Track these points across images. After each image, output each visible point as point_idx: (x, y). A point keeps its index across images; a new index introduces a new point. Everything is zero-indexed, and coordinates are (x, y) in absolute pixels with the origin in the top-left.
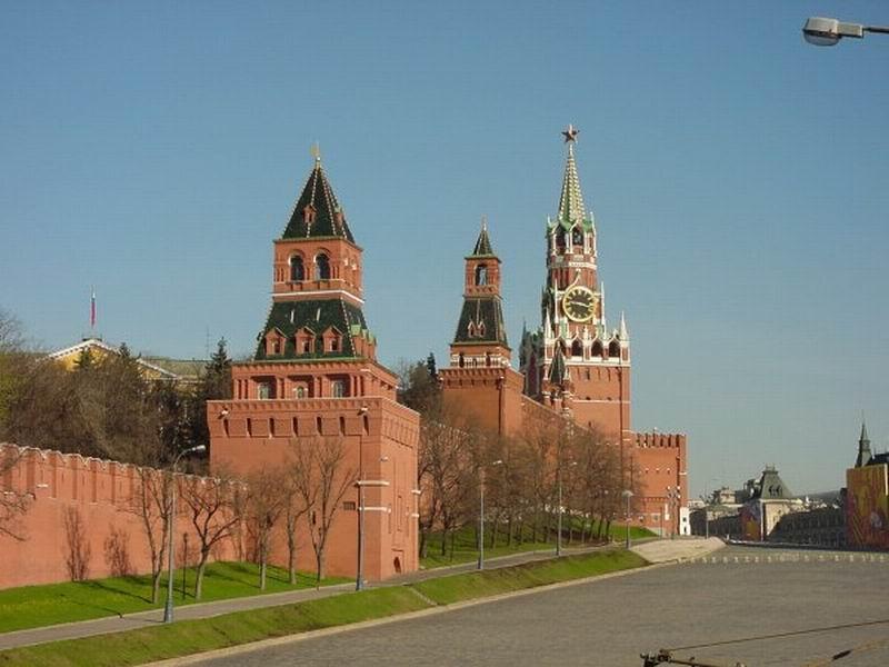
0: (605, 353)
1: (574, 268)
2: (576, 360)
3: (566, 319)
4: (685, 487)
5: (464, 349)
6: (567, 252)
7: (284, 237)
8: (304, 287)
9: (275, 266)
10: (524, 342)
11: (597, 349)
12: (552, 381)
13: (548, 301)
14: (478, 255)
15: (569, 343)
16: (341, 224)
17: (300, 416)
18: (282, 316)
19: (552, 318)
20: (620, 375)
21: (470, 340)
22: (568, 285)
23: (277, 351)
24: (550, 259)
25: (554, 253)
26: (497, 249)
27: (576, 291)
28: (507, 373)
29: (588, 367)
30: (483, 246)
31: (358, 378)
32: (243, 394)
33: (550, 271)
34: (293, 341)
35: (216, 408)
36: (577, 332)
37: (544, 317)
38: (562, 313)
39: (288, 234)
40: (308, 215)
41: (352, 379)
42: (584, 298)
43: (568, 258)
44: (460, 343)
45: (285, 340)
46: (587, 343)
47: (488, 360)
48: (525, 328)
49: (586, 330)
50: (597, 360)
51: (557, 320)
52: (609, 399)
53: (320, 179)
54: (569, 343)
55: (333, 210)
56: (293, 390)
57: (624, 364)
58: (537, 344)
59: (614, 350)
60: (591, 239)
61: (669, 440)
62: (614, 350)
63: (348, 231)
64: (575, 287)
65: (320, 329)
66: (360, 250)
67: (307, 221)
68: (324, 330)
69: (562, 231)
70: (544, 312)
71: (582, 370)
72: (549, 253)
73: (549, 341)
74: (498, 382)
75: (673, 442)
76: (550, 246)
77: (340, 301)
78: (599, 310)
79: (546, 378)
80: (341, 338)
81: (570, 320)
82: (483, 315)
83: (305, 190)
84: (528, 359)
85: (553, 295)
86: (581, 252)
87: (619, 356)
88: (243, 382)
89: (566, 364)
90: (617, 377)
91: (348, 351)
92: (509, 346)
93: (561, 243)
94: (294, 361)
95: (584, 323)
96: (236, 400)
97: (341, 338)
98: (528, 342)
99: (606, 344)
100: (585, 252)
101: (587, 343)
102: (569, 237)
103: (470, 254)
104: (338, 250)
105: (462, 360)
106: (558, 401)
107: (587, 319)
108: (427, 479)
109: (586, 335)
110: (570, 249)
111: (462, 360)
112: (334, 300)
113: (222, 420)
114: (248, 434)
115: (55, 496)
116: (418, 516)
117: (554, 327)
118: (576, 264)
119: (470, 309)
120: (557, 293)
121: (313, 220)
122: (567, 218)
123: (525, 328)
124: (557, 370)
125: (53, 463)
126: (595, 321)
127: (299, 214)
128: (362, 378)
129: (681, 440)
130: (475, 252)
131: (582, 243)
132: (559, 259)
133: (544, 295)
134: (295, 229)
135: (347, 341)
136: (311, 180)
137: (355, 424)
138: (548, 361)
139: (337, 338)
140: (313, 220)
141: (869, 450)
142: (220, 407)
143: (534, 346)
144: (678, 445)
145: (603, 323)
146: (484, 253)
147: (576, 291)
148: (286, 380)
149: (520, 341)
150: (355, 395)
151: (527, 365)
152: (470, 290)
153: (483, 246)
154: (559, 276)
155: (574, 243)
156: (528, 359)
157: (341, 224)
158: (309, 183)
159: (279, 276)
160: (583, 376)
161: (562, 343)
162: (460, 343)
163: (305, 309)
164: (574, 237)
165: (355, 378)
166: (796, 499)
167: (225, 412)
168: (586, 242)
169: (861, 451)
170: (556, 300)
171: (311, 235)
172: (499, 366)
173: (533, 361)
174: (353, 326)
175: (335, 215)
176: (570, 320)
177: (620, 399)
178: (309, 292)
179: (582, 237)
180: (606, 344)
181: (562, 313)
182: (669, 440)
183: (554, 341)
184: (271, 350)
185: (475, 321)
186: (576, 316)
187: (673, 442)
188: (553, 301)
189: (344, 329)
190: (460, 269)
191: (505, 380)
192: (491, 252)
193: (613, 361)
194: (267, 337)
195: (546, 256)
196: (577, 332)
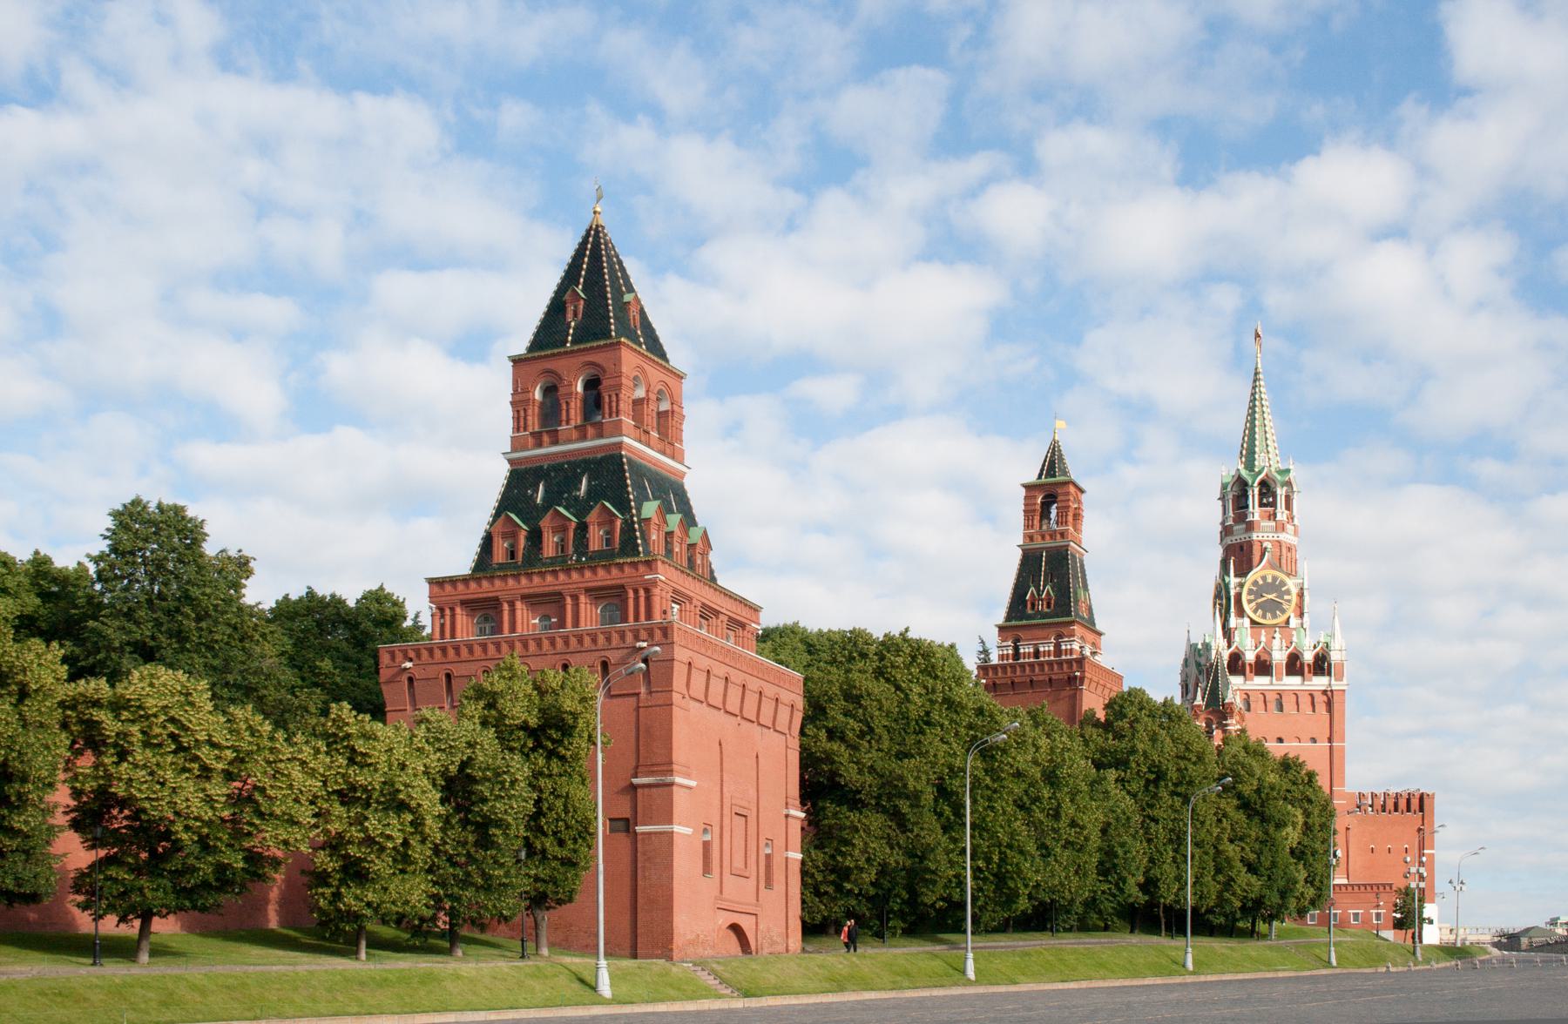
3: (1247, 621)
4: (1431, 871)
8: (561, 437)
11: (1294, 665)
12: (1207, 706)
13: (1221, 593)
20: (1329, 704)
21: (1030, 617)
22: (1250, 569)
23: (513, 555)
26: (1075, 469)
27: (1264, 578)
29: (1280, 694)
30: (1053, 463)
32: (448, 634)
34: (536, 537)
35: (393, 658)
36: (1263, 639)
38: (1241, 613)
39: (538, 343)
41: (631, 594)
42: (1276, 586)
43: (1250, 527)
44: (1013, 623)
46: (1279, 656)
47: (1058, 646)
49: (1277, 635)
50: (1294, 682)
52: (1314, 740)
53: (596, 245)
56: (528, 622)
57: (1336, 686)
58: (1203, 661)
59: (1321, 665)
61: (1408, 801)
62: (1321, 665)
65: (581, 509)
66: (1100, 634)
71: (1272, 698)
74: (1072, 680)
75: (1415, 803)
80: (619, 523)
81: (1253, 622)
90: (1324, 707)
91: (629, 545)
92: (1099, 627)
93: (1241, 502)
95: (1275, 626)
97: (619, 523)
99: (1308, 657)
101: (1279, 656)
103: (1032, 477)
104: (618, 363)
105: (1016, 649)
106: (1217, 734)
107: (1281, 619)
109: (1276, 643)
110: (1255, 512)
111: (1016, 649)
112: (612, 456)
113: (404, 678)
116: (800, 856)
119: (1029, 563)
120: (1233, 580)
122: (1250, 465)
126: (1294, 622)
127: (557, 308)
128: (647, 591)
130: (1040, 477)
131: (1274, 504)
134: (549, 333)
135: (628, 528)
142: (399, 656)
143: (1198, 665)
144: (1421, 809)
147: (1264, 578)
148: (519, 605)
150: (637, 619)
153: (1053, 463)
155: (1261, 505)
159: (519, 422)
160: (1272, 706)
162: (1013, 623)
163: (560, 476)
164: (1261, 494)
165: (636, 592)
167: (408, 665)
168: (1281, 502)
170: (1232, 593)
171: (573, 342)
175: (623, 307)
176: (1253, 622)
177: (1330, 740)
180: (1308, 657)
181: (1241, 613)
182: (1408, 801)
184: (499, 555)
186: (1264, 617)
187: (1415, 803)
188: (1228, 592)
189: (623, 506)
191: (1082, 679)
193: (1320, 682)
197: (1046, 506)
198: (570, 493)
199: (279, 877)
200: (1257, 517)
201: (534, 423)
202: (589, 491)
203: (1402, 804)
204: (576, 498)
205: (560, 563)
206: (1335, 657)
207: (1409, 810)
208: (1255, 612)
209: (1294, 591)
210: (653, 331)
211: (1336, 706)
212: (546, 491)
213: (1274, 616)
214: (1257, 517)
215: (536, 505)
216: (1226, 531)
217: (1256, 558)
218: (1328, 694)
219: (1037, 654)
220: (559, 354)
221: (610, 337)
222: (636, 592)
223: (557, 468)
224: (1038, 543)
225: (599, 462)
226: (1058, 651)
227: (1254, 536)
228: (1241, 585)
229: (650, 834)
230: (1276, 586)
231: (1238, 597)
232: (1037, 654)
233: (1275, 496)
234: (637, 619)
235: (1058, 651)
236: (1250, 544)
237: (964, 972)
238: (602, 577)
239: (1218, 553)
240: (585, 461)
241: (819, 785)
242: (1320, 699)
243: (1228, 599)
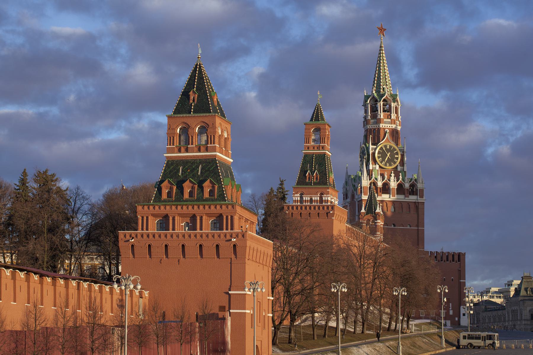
0: (406, 192)
1: (384, 129)
2: (385, 197)
3: (377, 166)
5: (304, 190)
6: (379, 117)
7: (175, 113)
10: (346, 183)
15: (380, 184)
16: (216, 104)
17: (204, 244)
19: (367, 165)
28: (335, 208)
31: (229, 217)
33: (367, 130)
38: (375, 162)
39: (177, 111)
43: (379, 121)
45: (175, 187)
47: (321, 198)
48: (347, 173)
51: (371, 167)
54: (380, 184)
57: (420, 200)
60: (396, 107)
61: (447, 257)
63: (221, 109)
64: (386, 142)
67: (191, 101)
68: (204, 181)
70: (362, 161)
72: (365, 117)
73: (365, 182)
75: (456, 258)
76: (366, 112)
77: (216, 160)
79: (363, 211)
80: (216, 187)
81: (380, 167)
82: (323, 200)
84: (349, 195)
85: (368, 149)
86: (389, 117)
87: (417, 194)
88: (145, 218)
89: (378, 199)
91: (222, 197)
93: (374, 110)
94: (182, 203)
96: (140, 231)
98: (350, 183)
100: (392, 118)
108: (280, 288)
109: (392, 178)
110: (382, 115)
111: (301, 197)
114: (131, 256)
115: (15, 301)
116: (271, 315)
118: (386, 126)
123: (347, 173)
124: (371, 205)
125: (28, 280)
129: (461, 257)
131: (389, 110)
133: (362, 148)
136: (195, 71)
137: (226, 251)
138: (365, 197)
139: (213, 187)
147: (385, 146)
149: (344, 182)
150: (142, 229)
151: (349, 200)
155: (384, 111)
156: (349, 195)
157: (216, 104)
161: (375, 184)
168: (393, 110)
170: (371, 153)
172: (329, 204)
173: (353, 196)
174: (226, 179)
179: (390, 106)
181: (375, 162)
182: (447, 257)
183: (369, 182)
187: (456, 258)
188: (368, 152)
189: (219, 182)
191: (333, 214)
195: (363, 120)
203: (450, 258)
206: (419, 186)
207: (453, 261)
214: (382, 117)
216: (366, 122)
217: (381, 138)
219: (311, 201)
220: (189, 117)
226: (321, 201)
227: (382, 125)
228: (375, 149)
231: (374, 154)
232: (311, 201)
234: (142, 229)
235: (321, 201)
236: (379, 129)
239: (362, 132)
243: (369, 155)
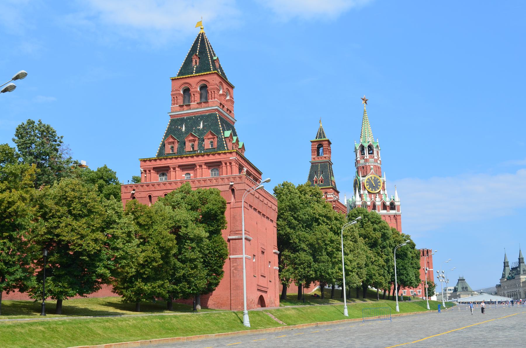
0: (388, 208)
3: (366, 192)
6: (365, 158)
7: (179, 75)
9: (172, 95)
11: (384, 207)
14: (318, 139)
18: (177, 130)
24: (357, 162)
25: (359, 159)
30: (321, 134)
36: (373, 198)
37: (355, 190)
40: (194, 61)
46: (378, 203)
49: (377, 196)
51: (362, 192)
53: (203, 39)
55: (212, 57)
59: (392, 206)
61: (423, 252)
62: (392, 206)
69: (362, 148)
70: (355, 190)
75: (425, 253)
78: (383, 187)
81: (368, 192)
83: (193, 47)
92: (338, 189)
99: (388, 204)
102: (366, 151)
109: (378, 199)
117: (361, 196)
118: (371, 163)
121: (198, 64)
126: (382, 192)
130: (316, 138)
131: (372, 153)
132: (362, 161)
134: (186, 69)
135: (220, 141)
140: (198, 64)
141: (508, 266)
145: (386, 193)
146: (321, 138)
147: (371, 177)
152: (314, 159)
153: (321, 134)
154: (362, 170)
155: (369, 154)
158: (194, 44)
159: (174, 97)
163: (192, 122)
164: (369, 150)
165: (226, 164)
166: (474, 292)
168: (375, 153)
169: (505, 267)
171: (196, 73)
178: (196, 108)
180: (388, 204)
182: (423, 252)
185: (317, 176)
186: (372, 190)
187: (425, 253)
190: (309, 147)
192: (325, 137)
193: (393, 212)
194: (166, 142)
196: (373, 198)
197: (318, 148)
198: (196, 127)
199: (109, 275)
200: (368, 157)
201: (180, 101)
202: (203, 127)
204: (199, 129)
205: (193, 154)
208: (369, 189)
209: (382, 182)
210: (223, 70)
211: (398, 220)
212: (185, 127)
213: (375, 190)
215: (182, 132)
218: (395, 216)
220: (191, 77)
221: (211, 71)
222: (226, 164)
223: (190, 119)
224: (317, 160)
225: (208, 116)
229: (236, 258)
230: (376, 180)
233: (373, 151)
237: (395, 309)
238: (212, 159)
240: (202, 116)
241: (283, 242)
242: (392, 217)
